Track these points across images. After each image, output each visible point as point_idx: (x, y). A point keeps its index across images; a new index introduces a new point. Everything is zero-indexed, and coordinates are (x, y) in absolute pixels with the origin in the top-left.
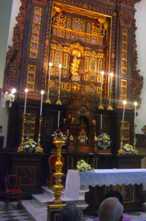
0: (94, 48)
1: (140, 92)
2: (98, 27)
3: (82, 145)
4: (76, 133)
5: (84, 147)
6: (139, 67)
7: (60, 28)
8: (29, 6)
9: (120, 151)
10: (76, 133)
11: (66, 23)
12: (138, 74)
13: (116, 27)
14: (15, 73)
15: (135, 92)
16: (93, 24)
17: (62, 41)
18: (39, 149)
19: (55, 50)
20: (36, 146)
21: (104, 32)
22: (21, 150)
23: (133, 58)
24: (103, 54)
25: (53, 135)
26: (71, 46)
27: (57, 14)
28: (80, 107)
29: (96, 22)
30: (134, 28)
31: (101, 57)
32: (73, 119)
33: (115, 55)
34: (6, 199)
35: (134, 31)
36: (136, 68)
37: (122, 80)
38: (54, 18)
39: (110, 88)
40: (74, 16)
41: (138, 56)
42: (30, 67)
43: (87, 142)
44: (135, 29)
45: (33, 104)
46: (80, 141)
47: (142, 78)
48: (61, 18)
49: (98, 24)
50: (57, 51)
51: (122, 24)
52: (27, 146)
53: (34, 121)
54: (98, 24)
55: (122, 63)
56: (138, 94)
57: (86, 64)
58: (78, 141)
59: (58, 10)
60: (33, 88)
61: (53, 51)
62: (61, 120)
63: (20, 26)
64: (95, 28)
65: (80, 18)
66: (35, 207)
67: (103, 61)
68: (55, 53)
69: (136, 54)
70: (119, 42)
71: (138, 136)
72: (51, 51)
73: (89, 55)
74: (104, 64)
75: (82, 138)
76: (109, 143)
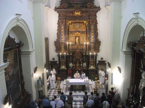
0: (83, 32)
1: (99, 47)
3: (77, 67)
4: (75, 64)
7: (71, 28)
9: (89, 68)
10: (75, 64)
18: (65, 68)
19: (70, 36)
23: (96, 35)
28: (77, 56)
29: (83, 23)
30: (96, 23)
34: (102, 107)
43: (79, 66)
45: (63, 56)
47: (100, 42)
51: (91, 23)
52: (62, 68)
56: (98, 47)
69: (98, 33)
71: (50, 61)
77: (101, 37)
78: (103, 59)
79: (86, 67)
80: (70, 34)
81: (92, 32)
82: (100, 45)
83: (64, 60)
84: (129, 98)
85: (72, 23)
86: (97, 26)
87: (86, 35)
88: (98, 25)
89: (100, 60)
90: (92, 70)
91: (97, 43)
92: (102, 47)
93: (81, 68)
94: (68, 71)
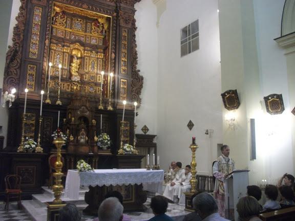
0: (94, 48)
2: (98, 27)
3: (82, 145)
4: (76, 133)
5: (84, 147)
6: (139, 67)
9: (120, 151)
10: (76, 133)
11: (66, 22)
12: (138, 75)
13: (116, 27)
17: (62, 41)
19: (55, 50)
20: (36, 146)
21: (104, 32)
22: (21, 150)
23: (133, 58)
24: (103, 54)
26: (71, 46)
27: (57, 14)
30: (134, 28)
32: (73, 119)
33: (115, 55)
35: (134, 31)
36: (136, 68)
37: (122, 80)
38: (54, 18)
40: (74, 16)
41: (138, 56)
43: (87, 142)
44: (135, 29)
46: (80, 141)
47: (142, 78)
52: (27, 146)
54: (98, 24)
56: (138, 94)
58: (78, 141)
59: (58, 9)
60: (33, 88)
63: (20, 26)
67: (103, 61)
75: (82, 138)
76: (109, 143)
77: (144, 66)
78: (148, 130)
79: (108, 148)
80: (57, 44)
81: (123, 46)
82: (141, 87)
83: (34, 118)
84: (65, 171)
85: (19, 179)
86: (134, 36)
87: (101, 56)
88: (136, 33)
89: (141, 133)
90: (30, 155)
91: (136, 84)
92: (145, 94)
93: (96, 148)
94: (50, 158)
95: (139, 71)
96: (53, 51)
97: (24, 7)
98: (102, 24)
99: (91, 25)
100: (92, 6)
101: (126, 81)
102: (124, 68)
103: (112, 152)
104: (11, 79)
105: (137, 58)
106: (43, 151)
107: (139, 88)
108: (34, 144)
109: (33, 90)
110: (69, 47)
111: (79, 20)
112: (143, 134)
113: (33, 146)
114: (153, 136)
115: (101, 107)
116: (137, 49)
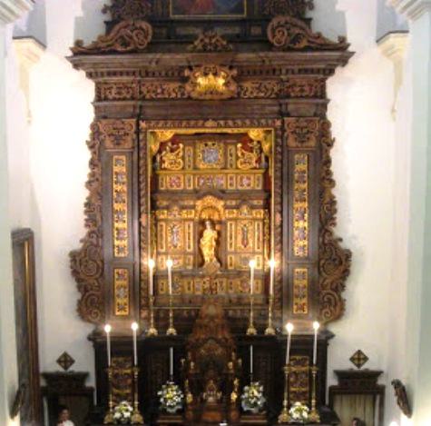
0: (243, 198)
3: (209, 409)
4: (198, 388)
5: (213, 414)
6: (338, 231)
8: (104, 158)
10: (198, 388)
12: (337, 248)
13: (282, 153)
14: (96, 284)
15: (332, 289)
16: (239, 145)
20: (132, 413)
21: (263, 159)
22: (110, 421)
23: (325, 211)
24: (262, 211)
25: (160, 393)
26: (199, 203)
28: (205, 341)
29: (244, 138)
30: (324, 140)
31: (258, 216)
32: (192, 364)
33: (282, 216)
35: (327, 151)
37: (297, 270)
38: (158, 158)
39: (284, 284)
41: (337, 207)
42: (118, 273)
43: (219, 401)
46: (206, 400)
47: (348, 255)
48: (172, 151)
49: (250, 145)
50: (171, 221)
51: (292, 142)
52: (117, 415)
53: (296, 187)
54: (250, 145)
55: (296, 233)
57: (231, 238)
58: (203, 401)
60: (127, 310)
61: (164, 224)
62: (177, 362)
63: (93, 200)
64: (243, 154)
65: (210, 140)
66: (399, 403)
67: (264, 224)
68: (167, 225)
69: (333, 202)
70: (288, 188)
72: (159, 224)
73: (235, 215)
74: (266, 230)
75: (210, 395)
76: (259, 403)
87: (260, 214)
95: (341, 240)
96: (164, 224)
97: (96, 162)
98: (259, 142)
99: (236, 149)
100: (233, 120)
101: (306, 270)
102: (301, 243)
103: (267, 416)
104: (89, 300)
105: (335, 211)
106: (320, 419)
107: (341, 278)
108: (127, 410)
109: (127, 313)
110: (194, 207)
111: (210, 143)
112: (355, 368)
113: (127, 415)
114: (377, 374)
115: (251, 331)
116: (335, 192)
